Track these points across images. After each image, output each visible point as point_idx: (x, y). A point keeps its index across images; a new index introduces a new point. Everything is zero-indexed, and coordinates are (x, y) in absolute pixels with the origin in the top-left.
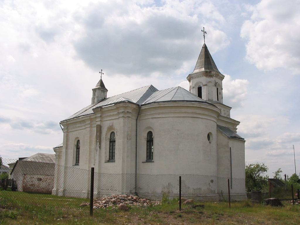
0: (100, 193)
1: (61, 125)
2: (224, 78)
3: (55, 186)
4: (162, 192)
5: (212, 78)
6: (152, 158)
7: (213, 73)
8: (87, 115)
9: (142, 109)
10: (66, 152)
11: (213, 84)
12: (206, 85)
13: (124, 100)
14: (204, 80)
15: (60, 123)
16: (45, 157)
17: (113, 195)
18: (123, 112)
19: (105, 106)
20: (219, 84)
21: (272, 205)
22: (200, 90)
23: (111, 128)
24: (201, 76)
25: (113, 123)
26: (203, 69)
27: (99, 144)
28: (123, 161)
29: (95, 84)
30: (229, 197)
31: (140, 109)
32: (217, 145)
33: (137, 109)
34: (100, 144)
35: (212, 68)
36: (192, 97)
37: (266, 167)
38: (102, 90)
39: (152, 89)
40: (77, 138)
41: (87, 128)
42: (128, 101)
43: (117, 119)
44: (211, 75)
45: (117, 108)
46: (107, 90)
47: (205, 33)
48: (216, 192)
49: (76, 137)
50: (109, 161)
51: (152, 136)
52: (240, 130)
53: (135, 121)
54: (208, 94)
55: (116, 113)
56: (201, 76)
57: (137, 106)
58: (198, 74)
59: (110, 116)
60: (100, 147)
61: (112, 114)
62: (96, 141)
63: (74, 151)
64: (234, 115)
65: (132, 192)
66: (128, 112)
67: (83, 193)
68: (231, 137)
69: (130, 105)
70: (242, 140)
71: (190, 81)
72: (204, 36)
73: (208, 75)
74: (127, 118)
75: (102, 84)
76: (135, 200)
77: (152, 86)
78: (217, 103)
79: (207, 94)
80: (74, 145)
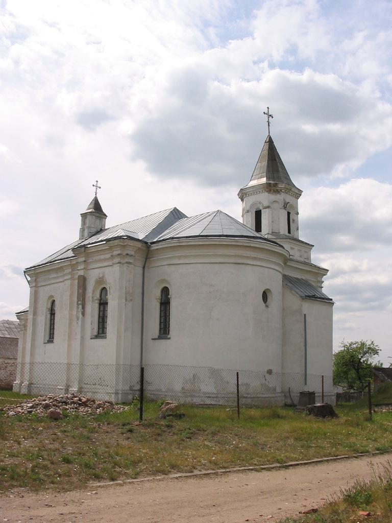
0: (83, 390)
1: (26, 275)
2: (301, 195)
3: (18, 376)
4: (183, 388)
5: (278, 195)
6: (168, 332)
7: (280, 186)
8: (67, 258)
9: (152, 249)
10: (34, 320)
11: (281, 205)
12: (268, 207)
13: (122, 233)
14: (265, 198)
15: (25, 272)
16: (13, 326)
17: (50, 395)
18: (119, 255)
19: (93, 243)
20: (292, 206)
21: (317, 415)
22: (258, 214)
23: (101, 280)
24: (260, 192)
25: (104, 272)
26: (264, 180)
27: (82, 308)
28: (119, 337)
29: (85, 206)
30: (238, 400)
31: (148, 251)
32: (284, 309)
33: (144, 249)
34: (83, 308)
35: (279, 178)
36: (238, 229)
37: (377, 348)
38: (97, 215)
39: (176, 215)
40: (52, 296)
41: (66, 280)
42: (127, 236)
43: (111, 266)
44: (277, 190)
45: (111, 248)
46: (106, 215)
47: (271, 118)
48: (278, 390)
49: (50, 294)
50: (97, 337)
51: (168, 295)
52: (328, 286)
53: (140, 270)
54: (271, 222)
55: (108, 256)
56: (260, 192)
57: (144, 245)
58: (255, 189)
59: (100, 261)
60: (83, 314)
61: (102, 257)
62: (77, 302)
63: (46, 318)
64: (319, 259)
65: (134, 389)
66: (127, 254)
67: (58, 389)
68: (306, 296)
69: (131, 243)
70: (328, 302)
71: (242, 200)
72: (268, 122)
73: (272, 191)
74: (126, 264)
75: (96, 205)
76: (83, 403)
77: (176, 210)
78: (287, 238)
79: (269, 222)
80: (47, 308)
